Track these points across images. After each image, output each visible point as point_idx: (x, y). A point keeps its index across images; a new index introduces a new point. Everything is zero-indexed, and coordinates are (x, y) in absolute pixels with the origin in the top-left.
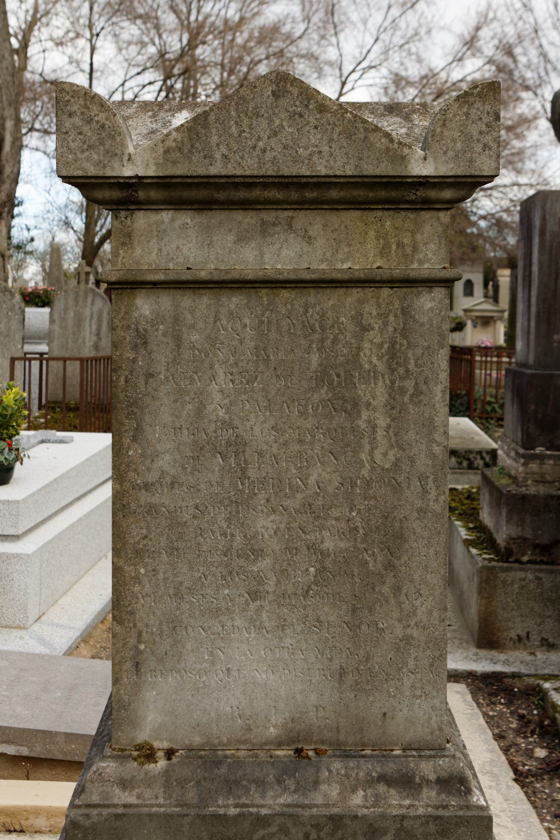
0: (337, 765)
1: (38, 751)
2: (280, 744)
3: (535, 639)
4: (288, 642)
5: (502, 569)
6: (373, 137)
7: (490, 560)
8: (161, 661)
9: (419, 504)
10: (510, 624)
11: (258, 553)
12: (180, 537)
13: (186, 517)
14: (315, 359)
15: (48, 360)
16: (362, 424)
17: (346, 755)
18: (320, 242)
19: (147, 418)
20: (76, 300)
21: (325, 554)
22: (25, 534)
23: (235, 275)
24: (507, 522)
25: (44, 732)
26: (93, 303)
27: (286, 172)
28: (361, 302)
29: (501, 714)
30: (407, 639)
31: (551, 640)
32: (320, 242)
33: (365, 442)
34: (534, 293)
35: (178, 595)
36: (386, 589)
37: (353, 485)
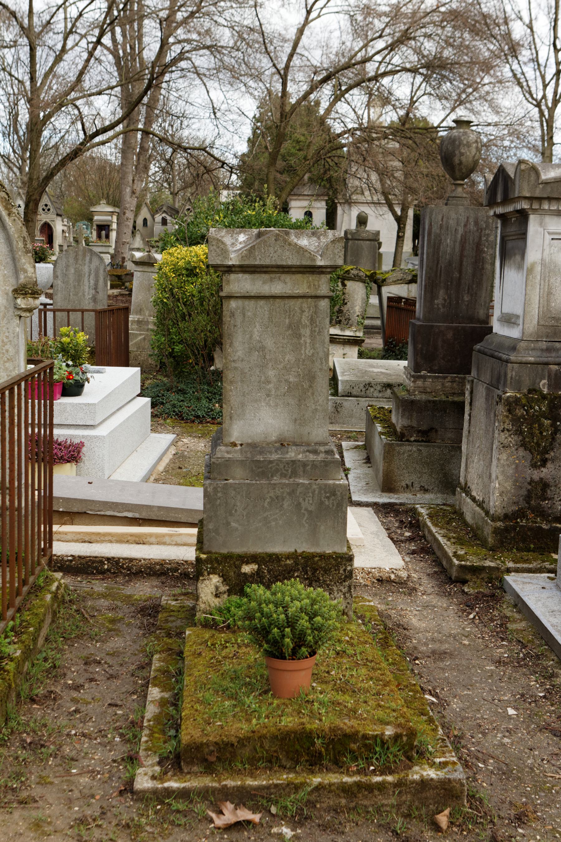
0: (294, 448)
1: (144, 515)
2: (276, 442)
3: (417, 486)
4: (278, 410)
5: (397, 444)
6: (306, 253)
7: (391, 441)
8: (239, 416)
9: (320, 367)
10: (402, 478)
11: (269, 382)
12: (244, 377)
13: (246, 371)
14: (287, 321)
15: (54, 311)
16: (302, 341)
17: (297, 445)
18: (289, 284)
19: (234, 339)
20: (76, 259)
21: (290, 383)
22: (101, 423)
23: (262, 295)
24: (402, 417)
25: (146, 506)
26: (90, 262)
27: (279, 264)
28: (302, 303)
29: (390, 522)
30: (316, 409)
31: (426, 487)
32: (289, 284)
33: (303, 347)
34: (424, 272)
35: (244, 395)
36: (309, 394)
37: (299, 361)
